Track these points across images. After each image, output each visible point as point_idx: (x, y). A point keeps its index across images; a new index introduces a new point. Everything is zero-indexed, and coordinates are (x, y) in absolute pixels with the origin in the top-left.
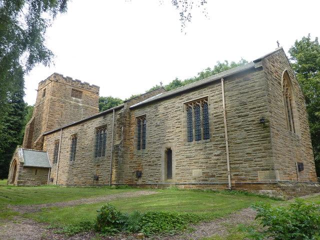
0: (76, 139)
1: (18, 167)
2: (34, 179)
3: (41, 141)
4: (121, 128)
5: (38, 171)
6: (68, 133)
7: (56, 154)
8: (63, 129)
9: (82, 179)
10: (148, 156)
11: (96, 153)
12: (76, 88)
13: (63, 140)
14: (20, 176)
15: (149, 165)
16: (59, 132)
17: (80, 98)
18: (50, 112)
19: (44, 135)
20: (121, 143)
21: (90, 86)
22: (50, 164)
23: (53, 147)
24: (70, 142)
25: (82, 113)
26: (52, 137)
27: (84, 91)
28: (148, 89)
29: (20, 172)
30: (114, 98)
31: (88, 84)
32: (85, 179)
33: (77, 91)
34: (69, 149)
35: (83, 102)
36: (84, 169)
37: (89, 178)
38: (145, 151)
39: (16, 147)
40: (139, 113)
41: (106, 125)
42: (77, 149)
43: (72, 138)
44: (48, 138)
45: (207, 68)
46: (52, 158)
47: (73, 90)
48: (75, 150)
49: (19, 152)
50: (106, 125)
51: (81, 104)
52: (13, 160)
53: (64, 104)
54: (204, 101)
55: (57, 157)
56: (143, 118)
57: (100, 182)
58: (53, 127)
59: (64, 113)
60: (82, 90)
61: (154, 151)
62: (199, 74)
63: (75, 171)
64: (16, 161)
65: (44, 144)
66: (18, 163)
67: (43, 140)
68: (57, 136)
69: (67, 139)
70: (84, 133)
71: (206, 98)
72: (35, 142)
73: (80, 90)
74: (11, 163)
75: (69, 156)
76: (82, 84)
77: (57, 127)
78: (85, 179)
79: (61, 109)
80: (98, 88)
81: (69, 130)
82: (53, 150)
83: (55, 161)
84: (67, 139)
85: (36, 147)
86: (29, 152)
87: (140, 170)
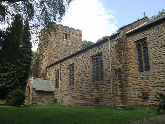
0: (73, 68)
1: (31, 91)
2: (43, 100)
3: (44, 72)
4: (121, 52)
5: (45, 94)
6: (65, 64)
7: (57, 81)
8: (62, 61)
9: (82, 100)
10: (155, 77)
11: (94, 78)
12: (65, 32)
13: (62, 70)
14: (33, 98)
15: (158, 86)
16: (58, 65)
17: (69, 39)
18: (49, 50)
19: (47, 68)
20: (123, 67)
21: (75, 30)
22: (53, 88)
23: (54, 76)
24: (68, 71)
25: (71, 50)
26: (53, 68)
27: (71, 34)
28: (135, 21)
29: (33, 95)
30: (88, 41)
31: (73, 29)
32: (85, 100)
33: (66, 34)
34: (67, 77)
35: (71, 42)
36: (83, 92)
37: (90, 99)
38: (151, 72)
39: (29, 77)
40: (139, 37)
41: (101, 53)
42: (75, 76)
43: (69, 67)
44: (50, 70)
45: (158, 12)
46: (54, 84)
47: (64, 33)
48: (73, 77)
49: (31, 80)
50: (101, 53)
51: (70, 44)
52: (27, 86)
53: (58, 44)
54: (144, 41)
55: (58, 83)
56: (144, 41)
57: (101, 103)
58: (52, 61)
59: (59, 50)
60: (70, 34)
61: (162, 71)
62: (159, 12)
63: (75, 94)
64: (29, 87)
65: (47, 74)
66: (31, 88)
67: (46, 71)
68: (56, 67)
69: (65, 69)
70: (80, 62)
71: (145, 38)
72: (41, 73)
73: (68, 33)
74: (26, 88)
75: (68, 81)
76: (69, 29)
77: (55, 61)
78: (85, 100)
79: (57, 48)
80: (81, 31)
81: (66, 61)
82: (54, 78)
83: (57, 86)
84: (65, 69)
85: (42, 76)
86: (38, 80)
87: (147, 91)
